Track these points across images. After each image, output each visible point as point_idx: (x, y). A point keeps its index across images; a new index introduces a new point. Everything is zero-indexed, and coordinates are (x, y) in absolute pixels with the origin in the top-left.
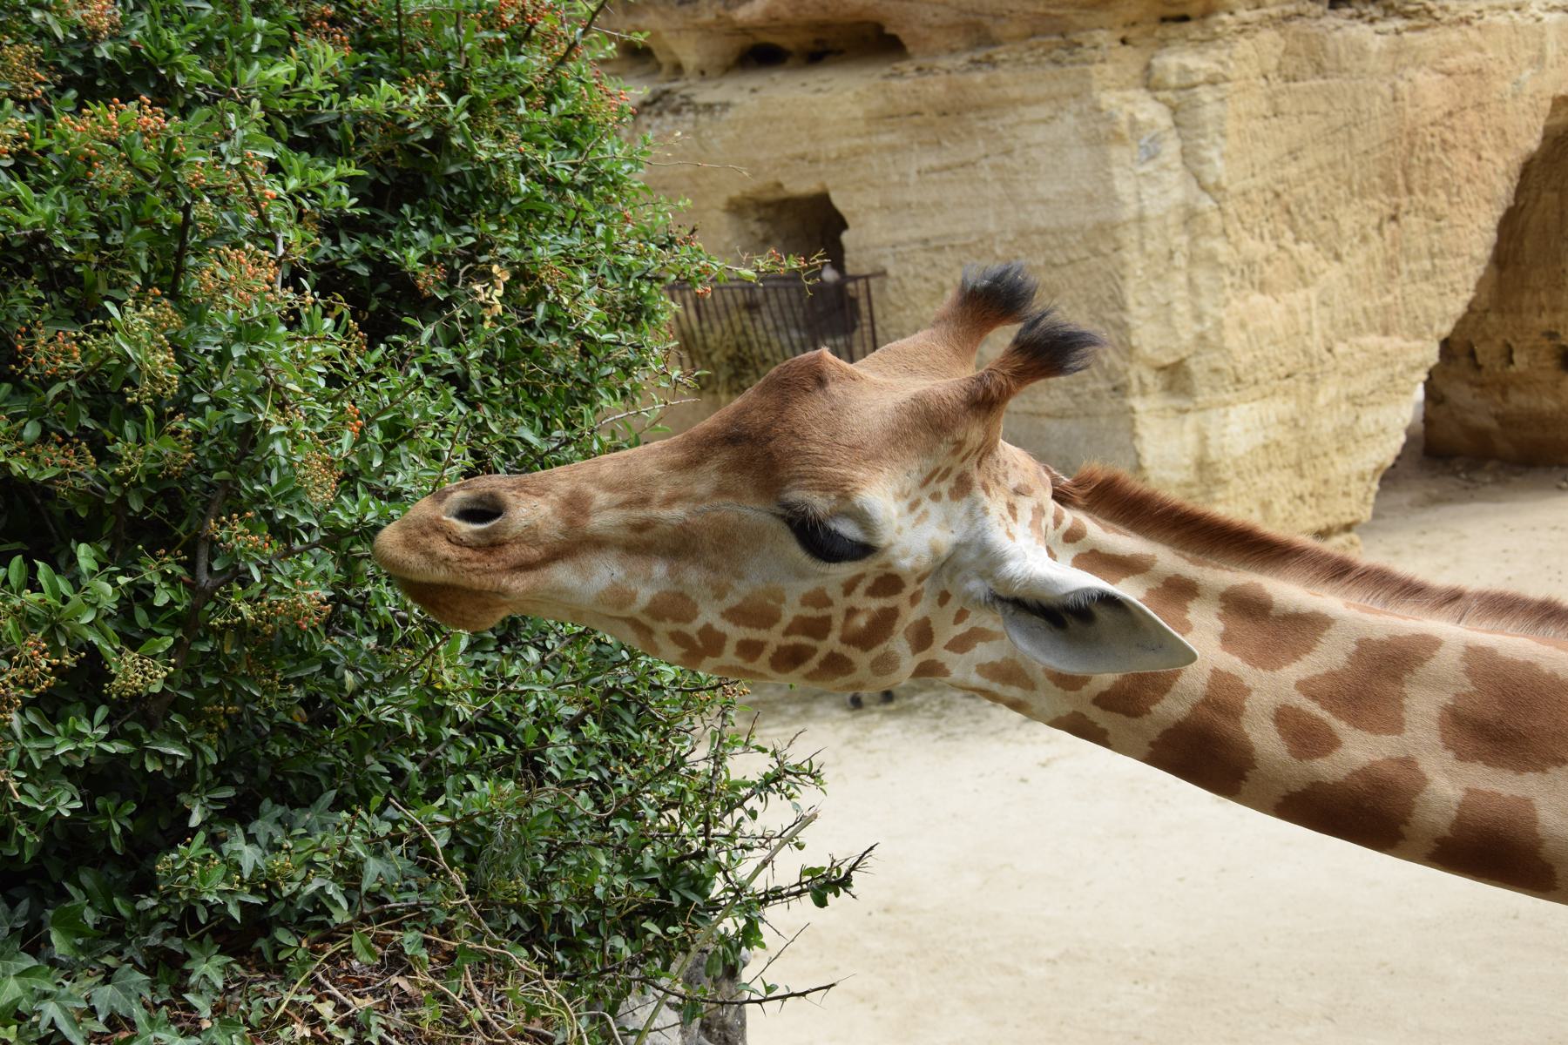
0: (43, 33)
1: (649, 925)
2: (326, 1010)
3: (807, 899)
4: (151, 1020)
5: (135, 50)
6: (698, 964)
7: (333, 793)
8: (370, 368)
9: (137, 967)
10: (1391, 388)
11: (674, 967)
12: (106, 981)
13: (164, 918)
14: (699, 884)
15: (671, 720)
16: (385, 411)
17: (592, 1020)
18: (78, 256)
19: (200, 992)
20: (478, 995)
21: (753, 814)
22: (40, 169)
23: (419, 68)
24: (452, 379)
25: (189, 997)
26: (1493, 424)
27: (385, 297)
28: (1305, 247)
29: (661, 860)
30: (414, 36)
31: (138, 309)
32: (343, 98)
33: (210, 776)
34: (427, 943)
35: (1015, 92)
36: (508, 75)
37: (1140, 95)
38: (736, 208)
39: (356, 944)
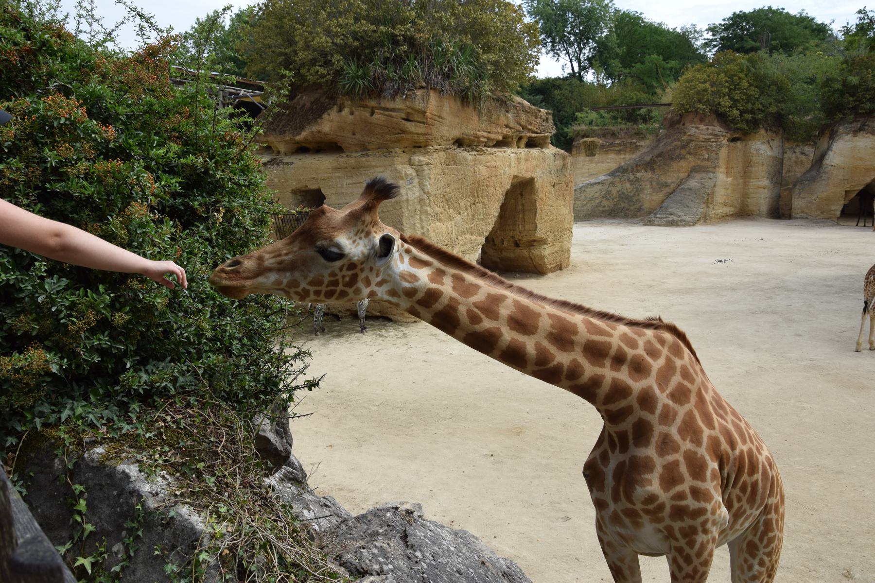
0: (95, 140)
1: (261, 396)
2: (168, 418)
3: (306, 389)
4: (119, 420)
5: (120, 145)
6: (276, 407)
7: (169, 358)
8: (184, 236)
9: (114, 405)
10: (473, 249)
11: (268, 407)
12: (106, 409)
13: (122, 392)
14: (276, 384)
15: (268, 338)
16: (187, 249)
17: (245, 422)
18: (101, 203)
19: (132, 413)
20: (212, 415)
21: (292, 365)
22: (91, 178)
23: (201, 151)
24: (207, 239)
25: (130, 414)
26: (498, 260)
27: (189, 215)
28: (451, 210)
29: (265, 378)
30: (200, 142)
31: (117, 218)
32: (179, 159)
33: (132, 353)
34: (197, 400)
35: (374, 164)
36: (227, 154)
37: (408, 166)
38: (294, 192)
39: (177, 400)
